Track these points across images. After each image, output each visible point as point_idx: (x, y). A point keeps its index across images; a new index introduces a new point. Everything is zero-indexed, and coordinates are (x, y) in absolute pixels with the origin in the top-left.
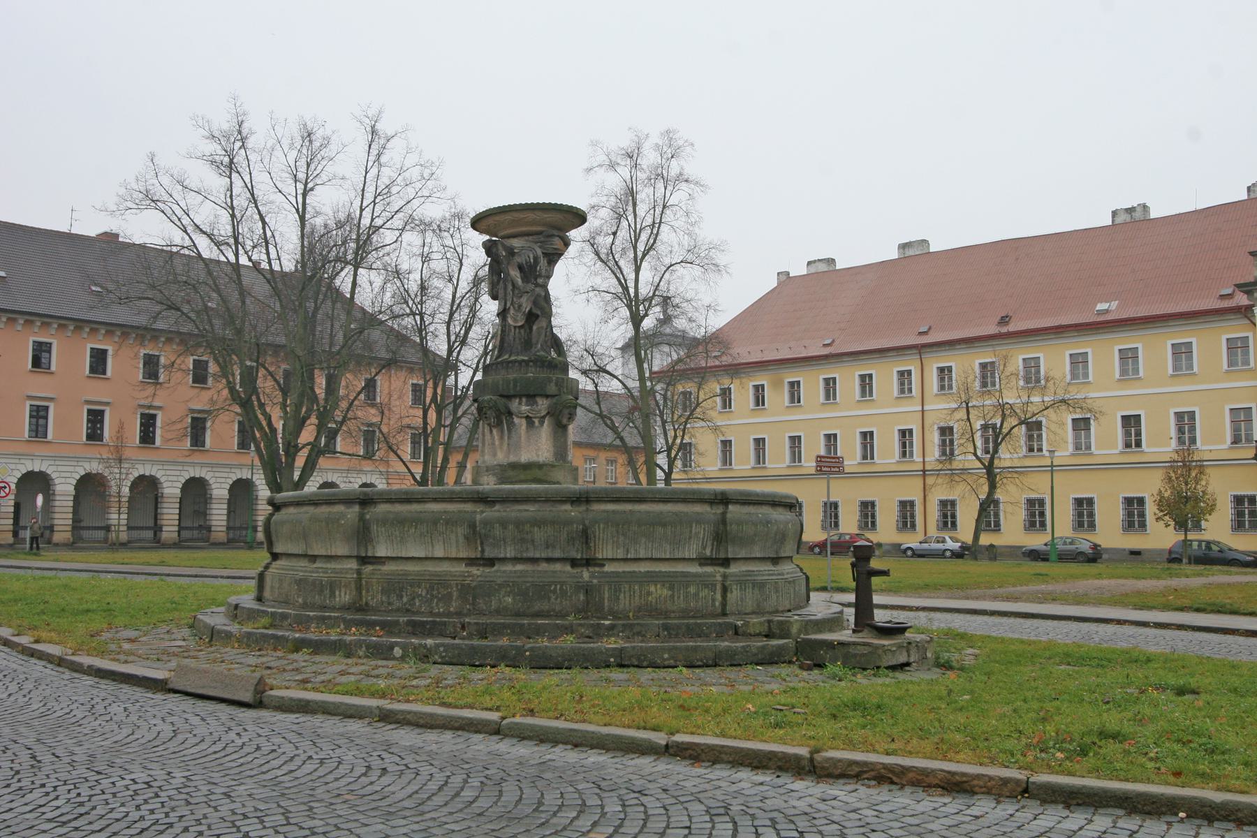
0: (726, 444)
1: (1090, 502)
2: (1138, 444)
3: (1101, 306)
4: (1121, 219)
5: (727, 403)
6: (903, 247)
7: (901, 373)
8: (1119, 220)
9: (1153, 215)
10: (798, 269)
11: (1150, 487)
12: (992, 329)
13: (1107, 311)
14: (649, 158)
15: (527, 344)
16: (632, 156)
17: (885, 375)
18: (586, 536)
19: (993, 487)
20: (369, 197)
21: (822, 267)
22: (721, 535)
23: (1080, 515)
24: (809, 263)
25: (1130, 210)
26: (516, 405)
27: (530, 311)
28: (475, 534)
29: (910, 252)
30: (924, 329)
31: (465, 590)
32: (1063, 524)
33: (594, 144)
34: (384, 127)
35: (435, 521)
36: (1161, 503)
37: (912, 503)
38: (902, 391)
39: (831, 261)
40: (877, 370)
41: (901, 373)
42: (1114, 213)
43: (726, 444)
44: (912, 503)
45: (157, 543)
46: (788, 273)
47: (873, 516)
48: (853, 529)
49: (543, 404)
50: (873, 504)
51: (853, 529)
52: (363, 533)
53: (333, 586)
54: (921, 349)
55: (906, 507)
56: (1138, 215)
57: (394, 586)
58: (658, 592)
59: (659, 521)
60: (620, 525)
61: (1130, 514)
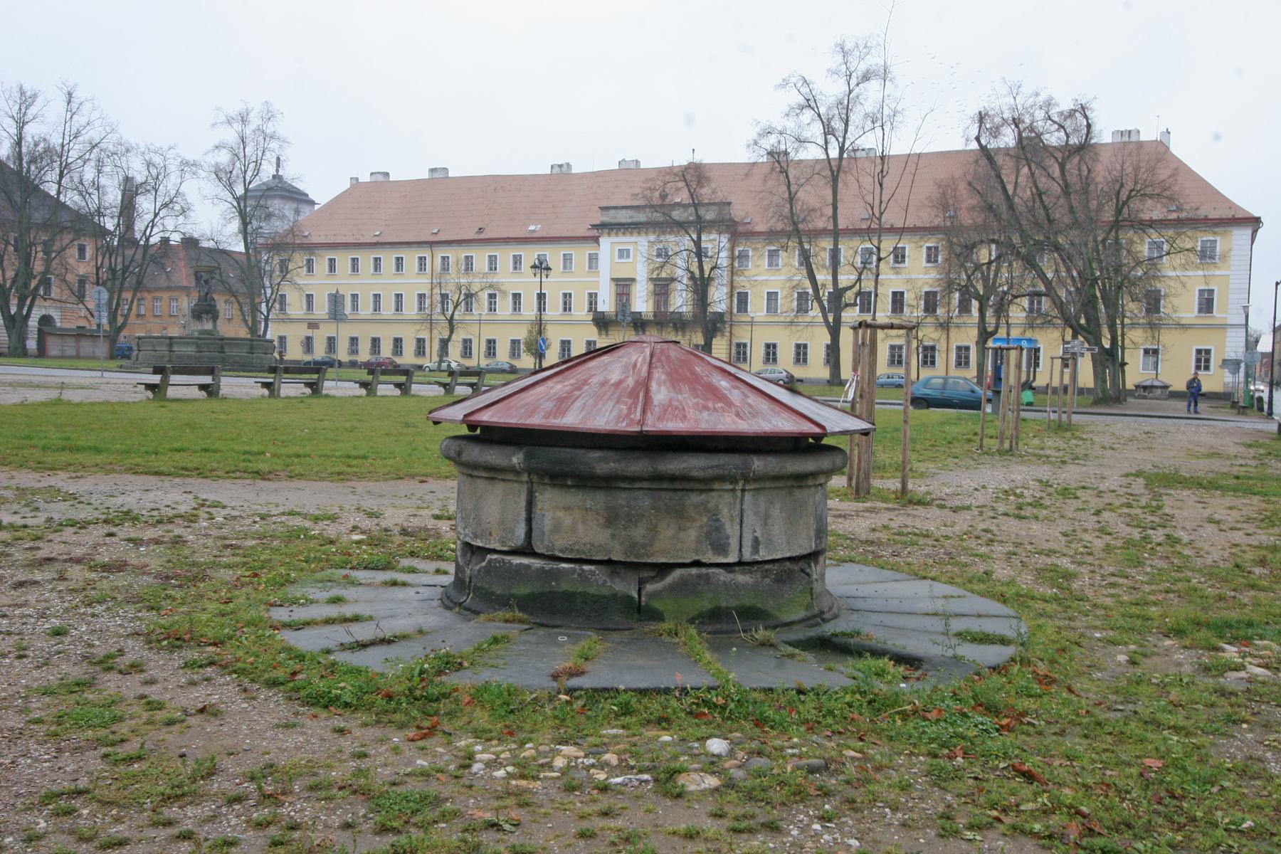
0: (310, 298)
1: (569, 342)
2: (570, 310)
3: (532, 228)
4: (556, 170)
5: (310, 269)
6: (432, 171)
7: (420, 258)
8: (554, 171)
9: (574, 171)
10: (365, 178)
11: (521, 334)
12: (472, 235)
13: (534, 231)
14: (255, 121)
15: (206, 300)
16: (244, 120)
17: (411, 258)
18: (222, 347)
19: (452, 332)
20: (67, 138)
21: (380, 178)
22: (252, 347)
23: (768, 354)
24: (372, 174)
25: (560, 166)
26: (204, 316)
27: (215, 318)
28: (198, 346)
29: (436, 175)
30: (435, 231)
31: (196, 358)
32: (386, 351)
33: (218, 109)
34: (79, 95)
35: (188, 343)
36: (526, 343)
37: (424, 340)
38: (421, 270)
39: (387, 174)
40: (405, 254)
41: (420, 258)
42: (552, 167)
43: (310, 298)
44: (424, 340)
46: (357, 179)
47: (494, 348)
48: (389, 355)
49: (210, 315)
50: (401, 340)
51: (389, 355)
52: (171, 345)
53: (163, 357)
54: (431, 244)
55: (420, 342)
56: (564, 169)
57: (179, 357)
58: (237, 359)
59: (238, 344)
60: (230, 345)
61: (798, 354)
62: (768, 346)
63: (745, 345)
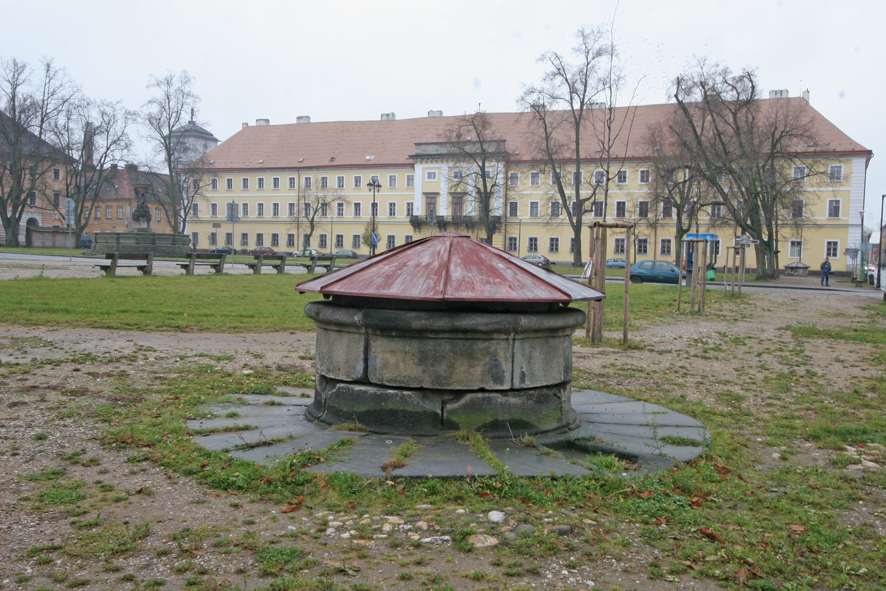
0: (214, 206)
1: (393, 237)
2: (394, 214)
3: (368, 158)
4: (385, 118)
5: (214, 186)
6: (299, 118)
7: (291, 179)
8: (383, 119)
9: (397, 118)
10: (253, 123)
11: (361, 231)
12: (326, 163)
13: (369, 160)
14: (176, 84)
15: (142, 207)
16: (169, 83)
17: (284, 178)
18: (154, 240)
19: (312, 230)
20: (46, 96)
21: (263, 123)
22: (174, 240)
23: (531, 245)
24: (257, 120)
25: (388, 115)
26: (141, 219)
27: (149, 220)
28: (137, 239)
29: (302, 121)
30: (301, 160)
31: (135, 247)
32: (267, 243)
33: (150, 75)
34: (55, 66)
35: (130, 237)
36: (364, 238)
37: (293, 235)
38: (291, 187)
39: (268, 121)
40: (280, 176)
41: (291, 179)
42: (382, 115)
43: (214, 206)
44: (293, 235)
45: (17, 245)
46: (247, 124)
47: (342, 241)
48: (269, 246)
49: (145, 218)
50: (277, 235)
51: (269, 246)
52: (118, 239)
53: (113, 247)
54: (298, 169)
55: (291, 237)
56: (390, 117)
57: (124, 247)
58: (164, 248)
59: (165, 238)
60: (159, 239)
61: (552, 245)
62: (531, 239)
63: (515, 239)
